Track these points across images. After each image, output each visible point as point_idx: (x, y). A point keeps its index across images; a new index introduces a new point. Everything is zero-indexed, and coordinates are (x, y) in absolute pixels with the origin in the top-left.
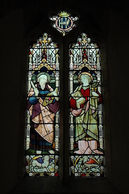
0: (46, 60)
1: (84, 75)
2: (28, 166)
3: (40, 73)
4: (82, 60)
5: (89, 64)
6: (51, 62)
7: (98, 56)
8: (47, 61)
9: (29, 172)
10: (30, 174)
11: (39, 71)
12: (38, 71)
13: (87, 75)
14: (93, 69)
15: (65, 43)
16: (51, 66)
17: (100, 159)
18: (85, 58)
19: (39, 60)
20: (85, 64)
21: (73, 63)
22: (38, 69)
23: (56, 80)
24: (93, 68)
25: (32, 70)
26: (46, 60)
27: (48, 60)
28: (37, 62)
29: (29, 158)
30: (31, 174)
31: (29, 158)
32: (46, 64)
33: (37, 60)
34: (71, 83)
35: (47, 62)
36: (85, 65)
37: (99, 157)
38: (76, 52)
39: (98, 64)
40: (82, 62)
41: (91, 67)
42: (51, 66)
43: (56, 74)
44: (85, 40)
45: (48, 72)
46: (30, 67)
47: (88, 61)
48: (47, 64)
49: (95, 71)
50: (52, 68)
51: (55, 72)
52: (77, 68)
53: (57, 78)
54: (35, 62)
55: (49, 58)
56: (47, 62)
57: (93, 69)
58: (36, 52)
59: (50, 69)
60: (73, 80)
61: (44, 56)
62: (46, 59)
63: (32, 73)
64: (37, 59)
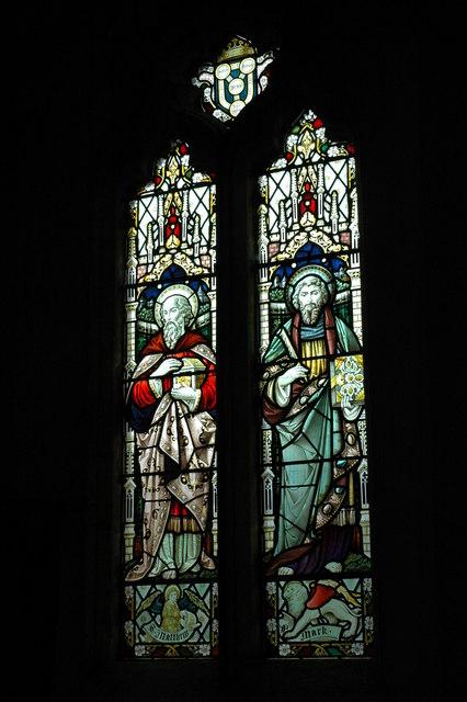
0: (180, 239)
1: (301, 282)
2: (274, 620)
3: (297, 268)
4: (296, 220)
5: (322, 231)
6: (334, 222)
7: (354, 195)
8: (182, 242)
9: (279, 643)
10: (281, 648)
11: (158, 282)
12: (287, 262)
13: (311, 278)
14: (336, 248)
15: (238, 157)
16: (197, 261)
17: (211, 631)
18: (308, 209)
19: (290, 221)
20: (173, 255)
21: (269, 233)
22: (288, 256)
23: (351, 291)
24: (337, 244)
25: (270, 264)
26: (180, 239)
27: (320, 216)
28: (283, 230)
29: (134, 629)
30: (285, 650)
31: (134, 629)
32: (179, 256)
33: (283, 222)
34: (265, 312)
35: (184, 246)
36: (173, 258)
37: (361, 582)
38: (279, 186)
39: (354, 227)
40: (296, 227)
41: (193, 262)
42: (197, 261)
43: (353, 266)
44: (304, 141)
45: (294, 265)
46: (264, 252)
47: (317, 219)
48: (183, 253)
49: (206, 276)
50: (201, 266)
51: (349, 260)
52: (280, 252)
53: (356, 283)
54: (275, 230)
55: (324, 208)
56: (320, 223)
57: (200, 269)
58: (149, 210)
59: (330, 249)
60: (271, 301)
61: (308, 203)
62: (315, 214)
63: (269, 272)
64: (283, 217)
